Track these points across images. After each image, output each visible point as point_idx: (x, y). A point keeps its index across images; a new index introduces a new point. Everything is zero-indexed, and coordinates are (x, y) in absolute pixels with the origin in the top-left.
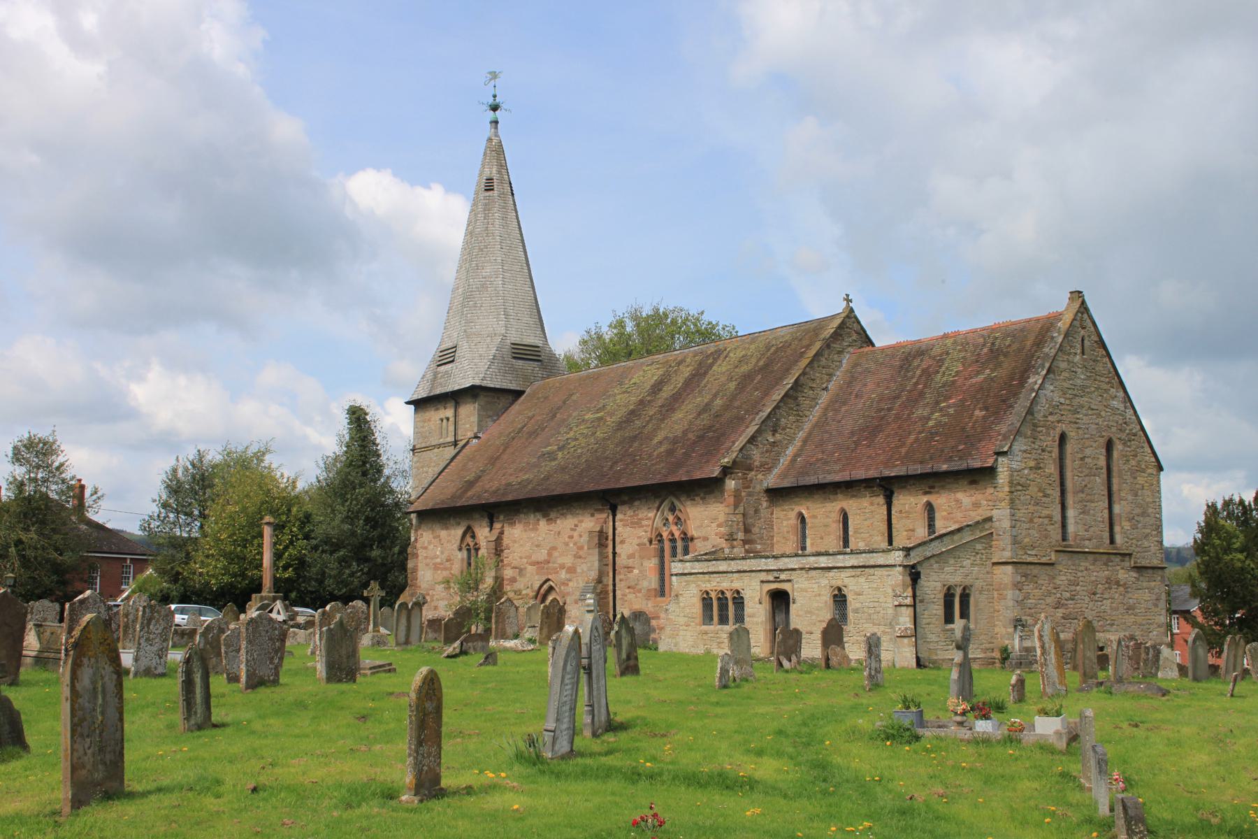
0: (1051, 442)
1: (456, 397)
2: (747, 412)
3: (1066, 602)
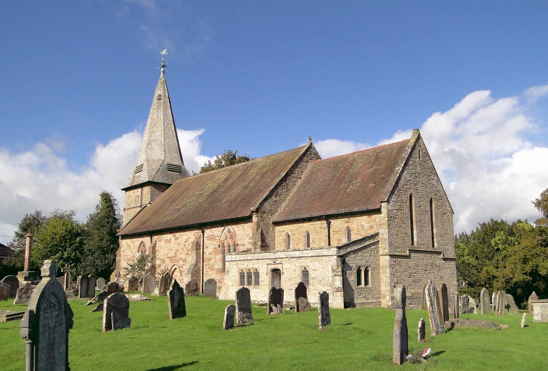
0: (406, 198)
1: (142, 186)
2: (264, 187)
3: (414, 274)
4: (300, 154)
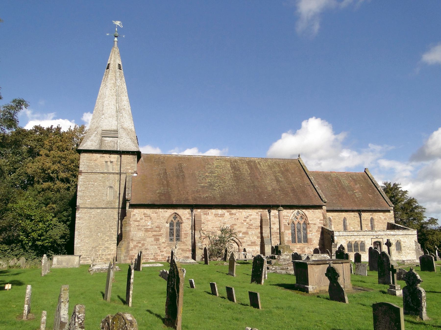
4: (112, 139)
